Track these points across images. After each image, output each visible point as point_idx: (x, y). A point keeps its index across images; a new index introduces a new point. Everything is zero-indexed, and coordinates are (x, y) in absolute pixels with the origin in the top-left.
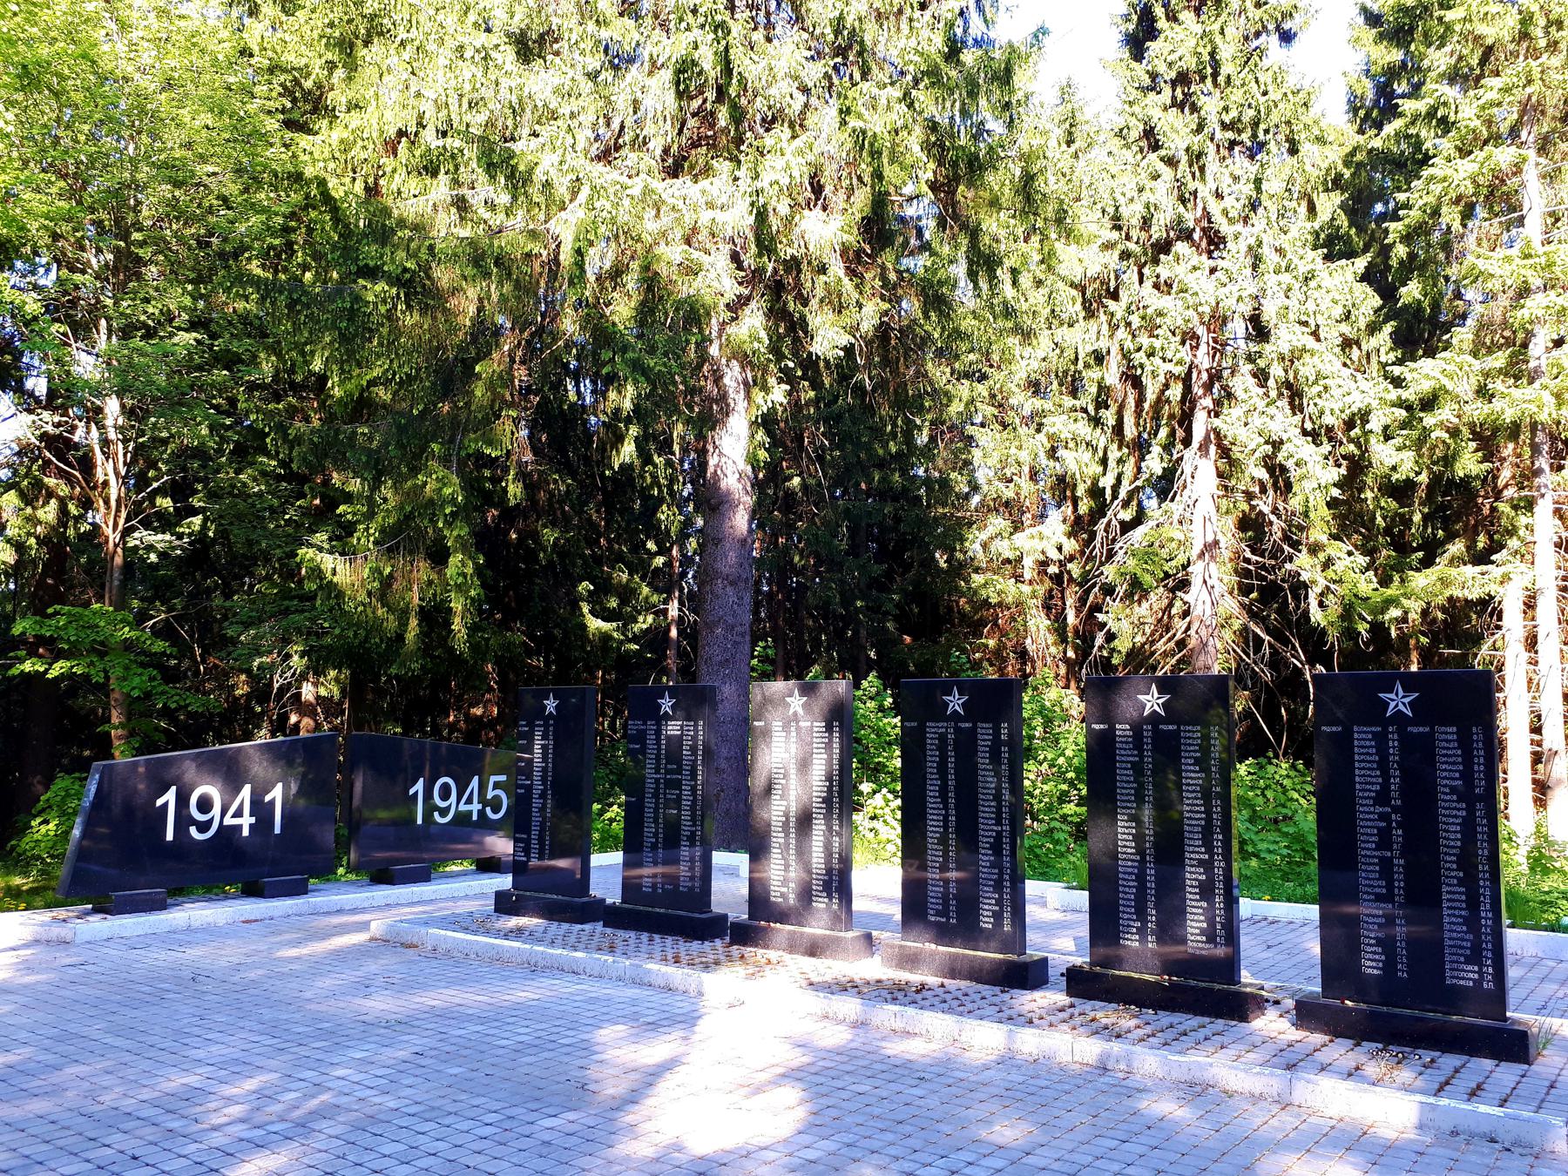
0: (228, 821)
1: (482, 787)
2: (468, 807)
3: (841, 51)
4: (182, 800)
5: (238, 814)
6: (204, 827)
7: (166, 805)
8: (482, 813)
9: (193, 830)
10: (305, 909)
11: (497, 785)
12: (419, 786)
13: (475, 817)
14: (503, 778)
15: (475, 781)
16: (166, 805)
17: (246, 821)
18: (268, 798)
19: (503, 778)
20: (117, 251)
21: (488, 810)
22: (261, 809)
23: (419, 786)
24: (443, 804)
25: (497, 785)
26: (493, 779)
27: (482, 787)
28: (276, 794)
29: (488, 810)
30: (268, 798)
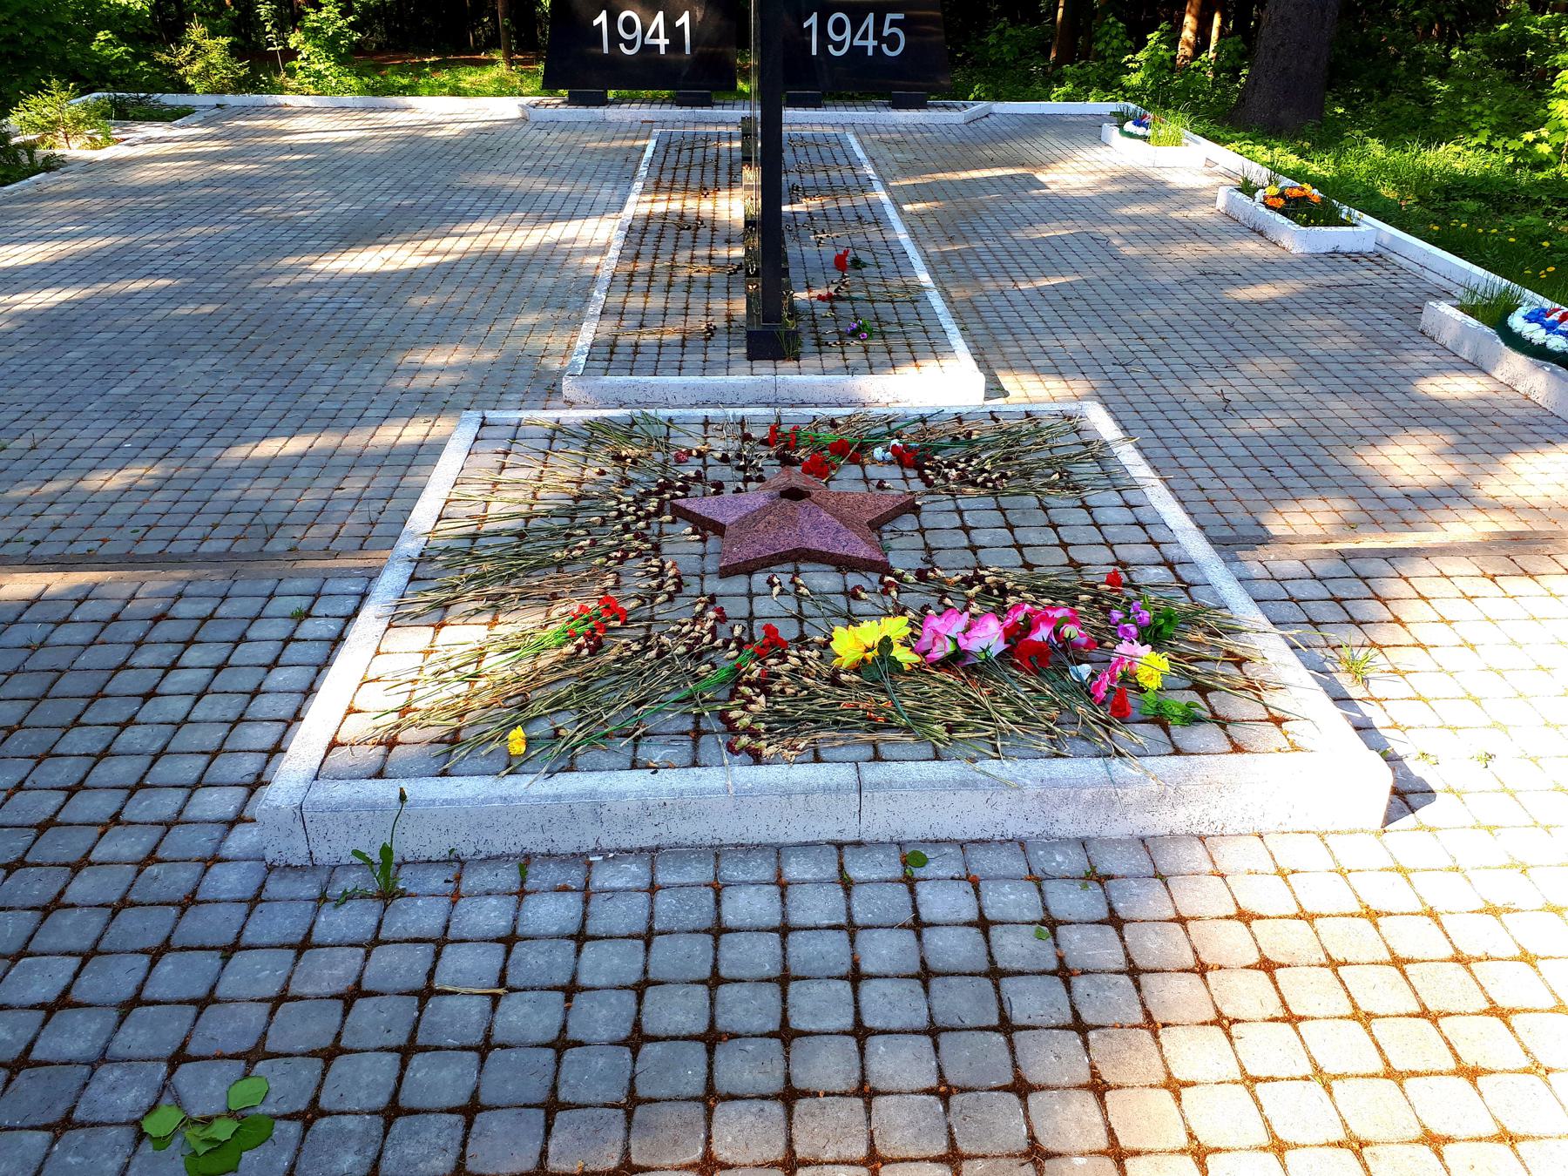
0: (857, 42)
1: (879, 23)
2: (656, 42)
3: (709, 330)
4: (612, 20)
5: (656, 35)
6: (630, 44)
7: (810, 27)
8: (877, 49)
9: (830, 47)
10: (692, 118)
11: (893, 23)
12: (602, 19)
13: (870, 53)
14: (901, 16)
15: (870, 19)
16: (810, 27)
17: (663, 42)
18: (678, 23)
19: (901, 16)
20: (698, 473)
21: (884, 47)
22: (674, 33)
23: (602, 19)
24: (838, 39)
25: (893, 23)
26: (889, 17)
27: (879, 23)
28: (685, 19)
29: (884, 47)
30: (678, 23)
